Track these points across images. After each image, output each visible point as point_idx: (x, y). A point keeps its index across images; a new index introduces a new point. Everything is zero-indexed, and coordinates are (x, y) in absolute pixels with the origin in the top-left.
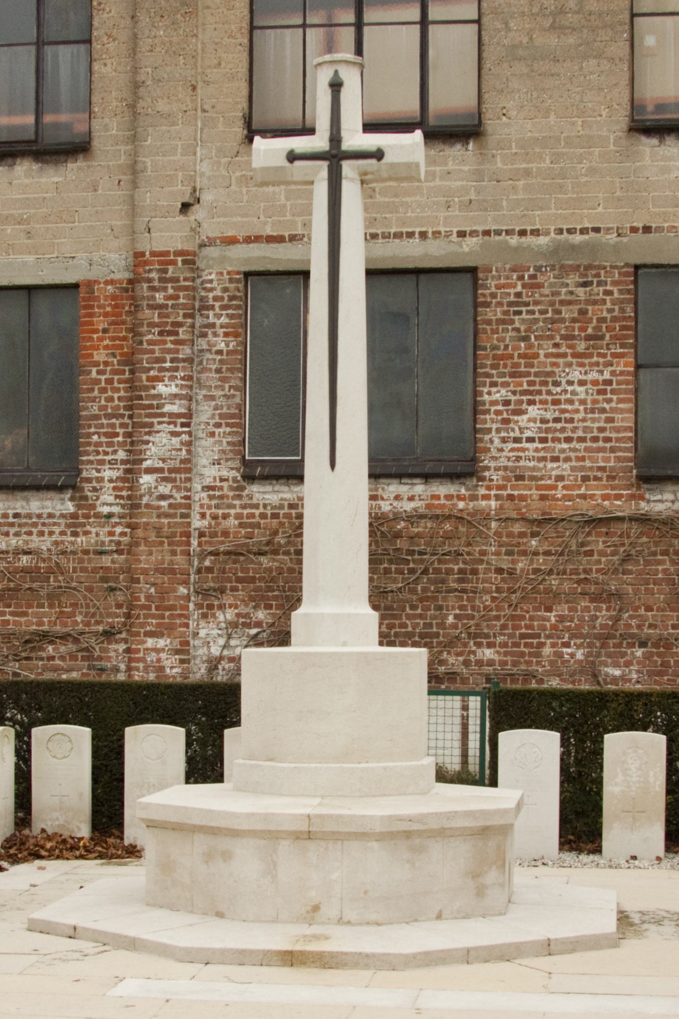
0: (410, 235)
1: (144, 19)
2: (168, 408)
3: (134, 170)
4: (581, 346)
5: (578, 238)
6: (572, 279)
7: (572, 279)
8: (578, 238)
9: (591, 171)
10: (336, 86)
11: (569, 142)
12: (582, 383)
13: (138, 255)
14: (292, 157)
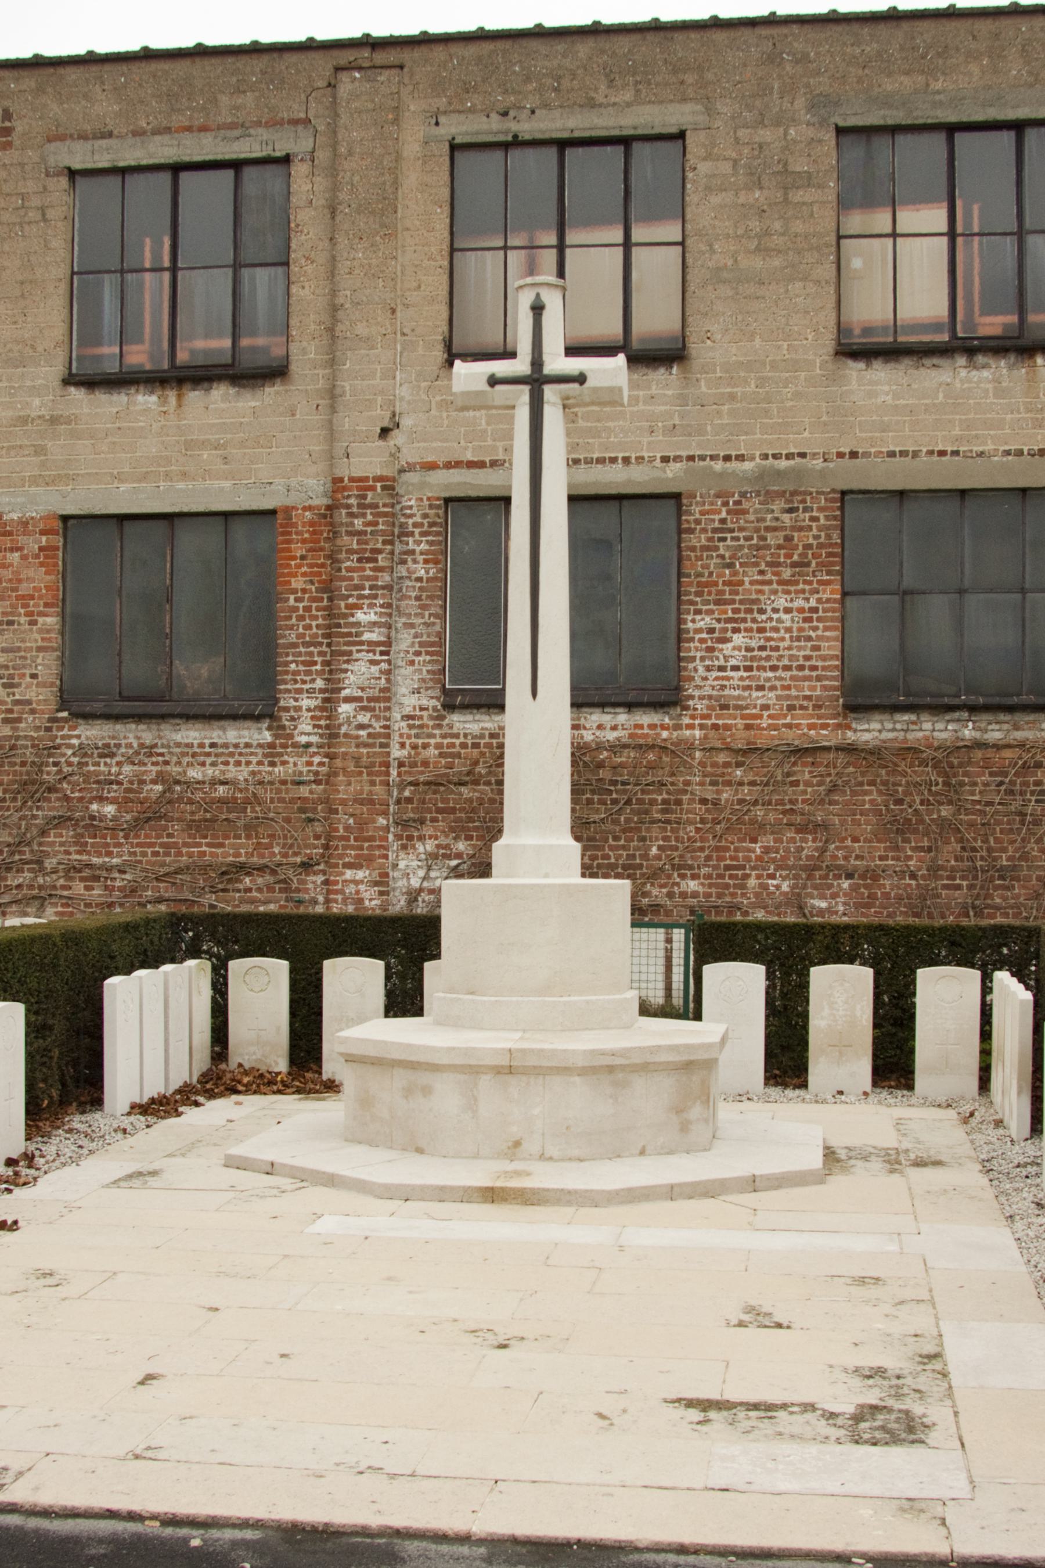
0: (613, 460)
1: (342, 241)
2: (367, 636)
3: (332, 394)
4: (787, 573)
5: (783, 464)
7: (778, 505)
8: (783, 464)
9: (798, 395)
10: (538, 309)
11: (774, 366)
12: (787, 611)
14: (493, 381)
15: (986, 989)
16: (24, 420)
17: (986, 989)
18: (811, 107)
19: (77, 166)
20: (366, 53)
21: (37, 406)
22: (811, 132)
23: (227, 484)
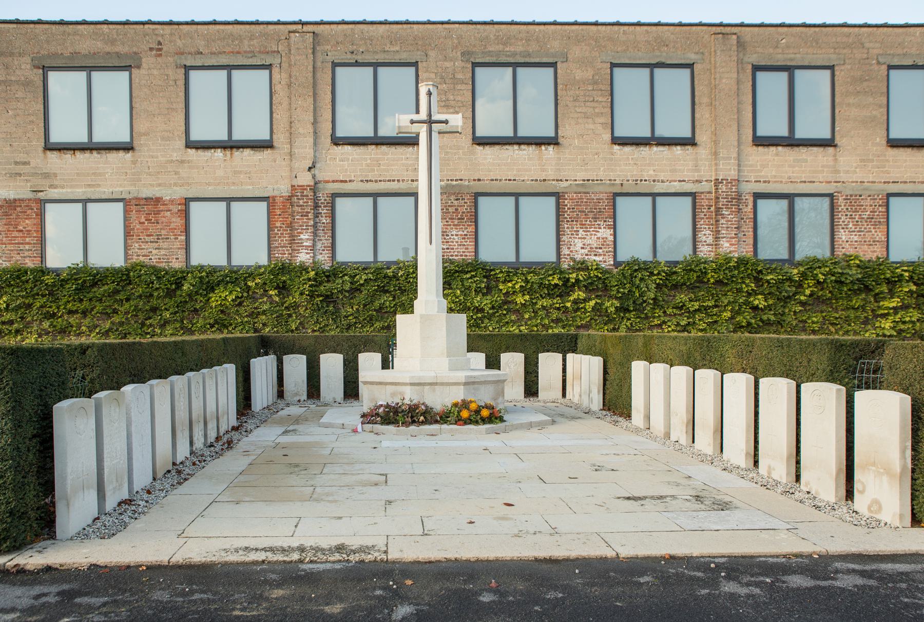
0: (394, 181)
1: (293, 98)
2: (305, 244)
3: (291, 154)
4: (456, 222)
5: (454, 183)
6: (453, 198)
7: (453, 198)
8: (454, 183)
9: (459, 158)
10: (429, 94)
11: (451, 148)
12: (457, 235)
13: (293, 186)
14: (412, 122)
15: (564, 360)
16: (172, 161)
17: (564, 360)
18: (463, 54)
19: (188, 64)
20: (300, 26)
21: (175, 156)
22: (463, 64)
23: (251, 187)
